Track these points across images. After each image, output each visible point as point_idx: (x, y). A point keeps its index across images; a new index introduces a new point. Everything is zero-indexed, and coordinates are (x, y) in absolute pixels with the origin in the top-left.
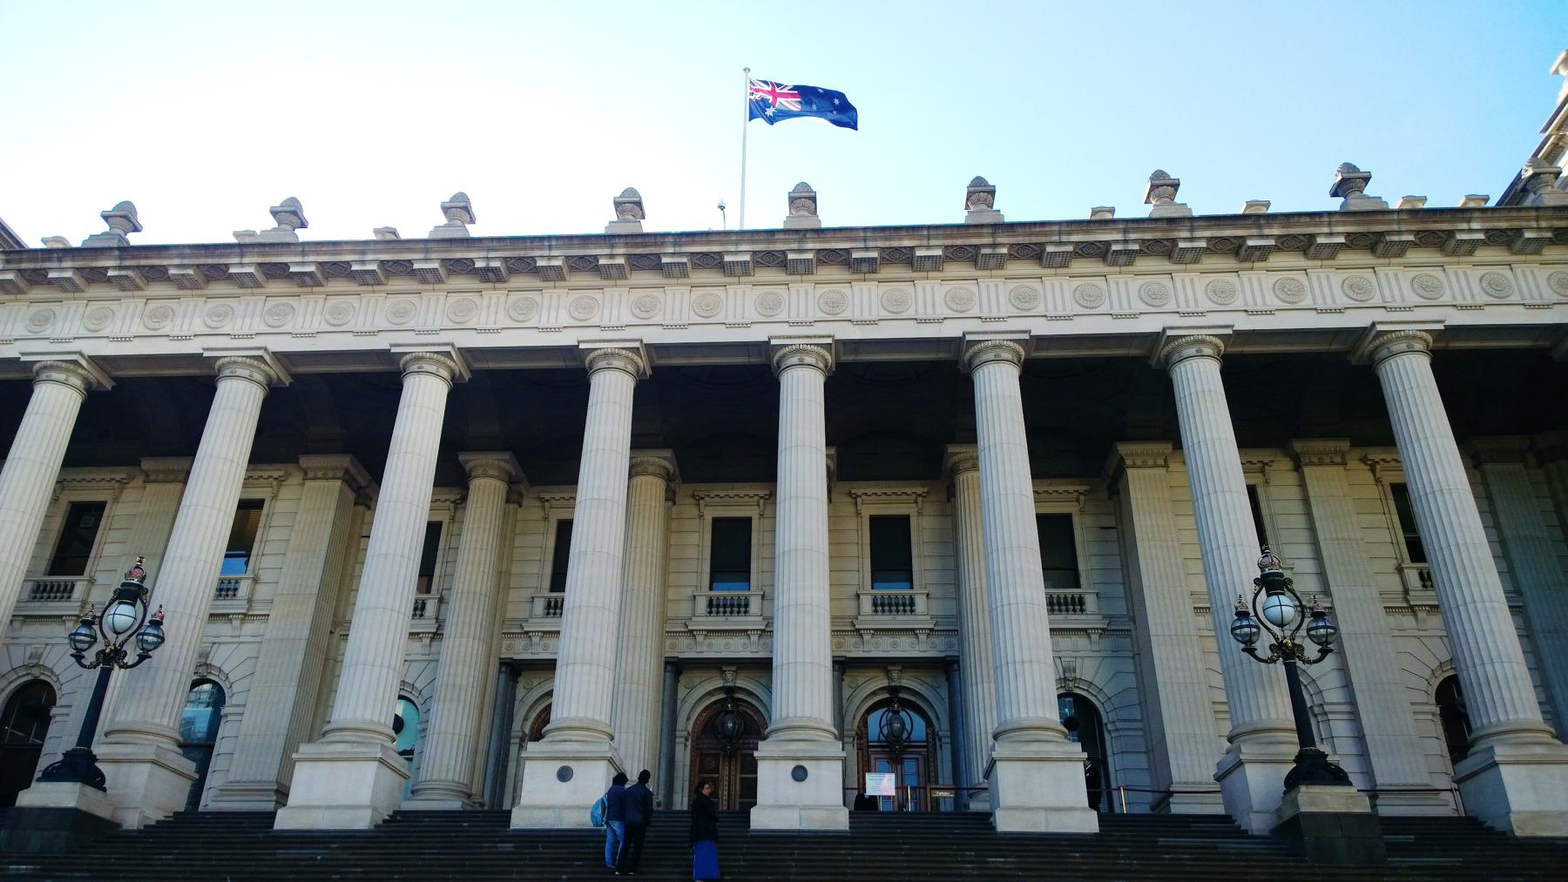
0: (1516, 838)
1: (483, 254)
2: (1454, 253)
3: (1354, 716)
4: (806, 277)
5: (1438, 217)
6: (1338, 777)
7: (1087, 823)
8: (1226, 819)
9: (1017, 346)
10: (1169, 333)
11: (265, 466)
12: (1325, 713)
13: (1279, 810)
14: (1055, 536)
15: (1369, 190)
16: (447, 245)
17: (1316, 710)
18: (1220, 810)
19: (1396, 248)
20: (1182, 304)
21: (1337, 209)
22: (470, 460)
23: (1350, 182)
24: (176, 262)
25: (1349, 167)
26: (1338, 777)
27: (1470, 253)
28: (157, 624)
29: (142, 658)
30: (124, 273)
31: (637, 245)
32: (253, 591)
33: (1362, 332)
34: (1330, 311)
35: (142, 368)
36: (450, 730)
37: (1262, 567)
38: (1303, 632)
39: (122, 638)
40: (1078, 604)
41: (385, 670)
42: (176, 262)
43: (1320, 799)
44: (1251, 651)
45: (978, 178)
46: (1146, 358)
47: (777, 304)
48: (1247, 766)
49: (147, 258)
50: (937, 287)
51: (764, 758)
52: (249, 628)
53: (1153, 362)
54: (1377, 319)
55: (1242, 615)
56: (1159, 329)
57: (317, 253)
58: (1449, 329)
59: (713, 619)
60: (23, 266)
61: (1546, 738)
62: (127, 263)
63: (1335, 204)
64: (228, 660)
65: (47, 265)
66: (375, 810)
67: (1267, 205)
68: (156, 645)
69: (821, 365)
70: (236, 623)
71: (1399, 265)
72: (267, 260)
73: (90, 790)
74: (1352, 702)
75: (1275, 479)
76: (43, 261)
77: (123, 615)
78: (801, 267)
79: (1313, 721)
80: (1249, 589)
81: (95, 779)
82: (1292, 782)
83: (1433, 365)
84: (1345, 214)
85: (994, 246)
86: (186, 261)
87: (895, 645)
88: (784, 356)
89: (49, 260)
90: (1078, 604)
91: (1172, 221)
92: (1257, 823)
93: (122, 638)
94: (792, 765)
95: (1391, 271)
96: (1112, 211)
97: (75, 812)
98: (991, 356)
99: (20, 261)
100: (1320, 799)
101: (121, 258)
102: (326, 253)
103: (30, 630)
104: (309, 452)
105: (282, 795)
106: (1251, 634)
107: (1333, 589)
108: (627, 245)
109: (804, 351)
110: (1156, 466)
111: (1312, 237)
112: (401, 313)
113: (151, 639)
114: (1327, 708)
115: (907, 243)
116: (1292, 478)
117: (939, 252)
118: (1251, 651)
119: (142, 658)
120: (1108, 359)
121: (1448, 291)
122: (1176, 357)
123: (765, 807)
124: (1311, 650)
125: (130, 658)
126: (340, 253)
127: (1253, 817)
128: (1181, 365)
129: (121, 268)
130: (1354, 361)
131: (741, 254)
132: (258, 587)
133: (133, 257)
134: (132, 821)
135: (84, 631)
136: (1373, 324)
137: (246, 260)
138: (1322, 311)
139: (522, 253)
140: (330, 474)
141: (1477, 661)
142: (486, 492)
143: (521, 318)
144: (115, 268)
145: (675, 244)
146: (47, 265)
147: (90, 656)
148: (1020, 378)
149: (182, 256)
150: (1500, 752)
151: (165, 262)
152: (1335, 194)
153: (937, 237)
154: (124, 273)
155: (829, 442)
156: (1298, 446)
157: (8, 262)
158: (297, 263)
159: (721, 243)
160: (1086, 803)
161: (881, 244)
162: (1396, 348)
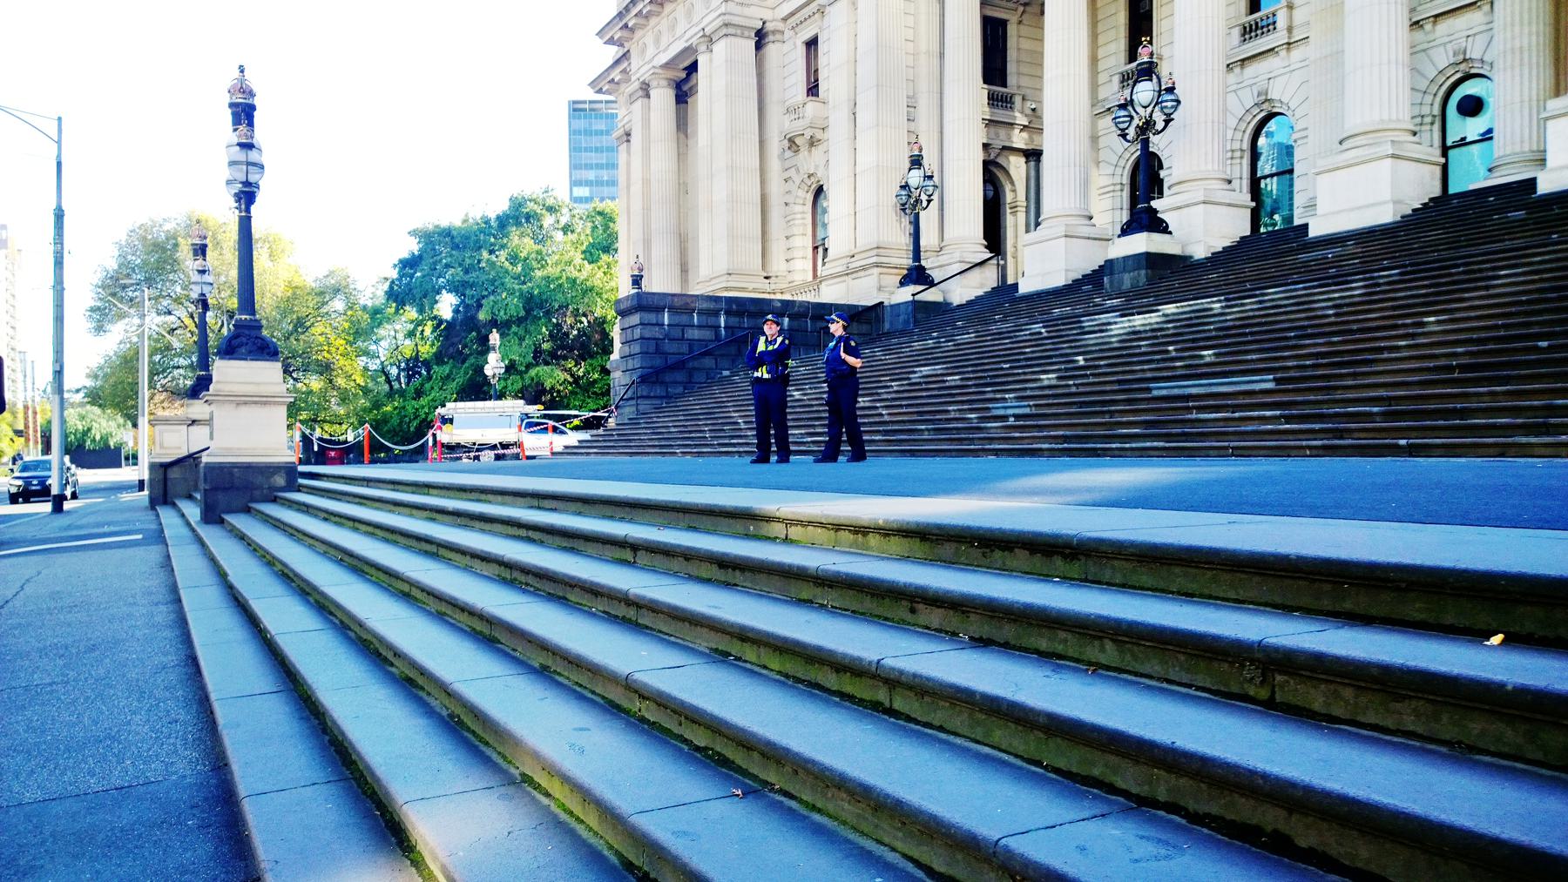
17: (1238, 154)
28: (1171, 90)
29: (1167, 122)
32: (1291, 18)
36: (1517, 99)
41: (1393, 66)
44: (1124, 136)
52: (1297, 53)
66: (1395, 202)
68: (1176, 108)
70: (1283, 53)
73: (1155, 236)
77: (1145, 92)
81: (1159, 226)
97: (1148, 255)
103: (1252, 69)
105: (1542, 162)
113: (1169, 104)
119: (1167, 122)
125: (1160, 126)
132: (1295, 12)
134: (1200, 252)
135: (1123, 113)
147: (1131, 132)
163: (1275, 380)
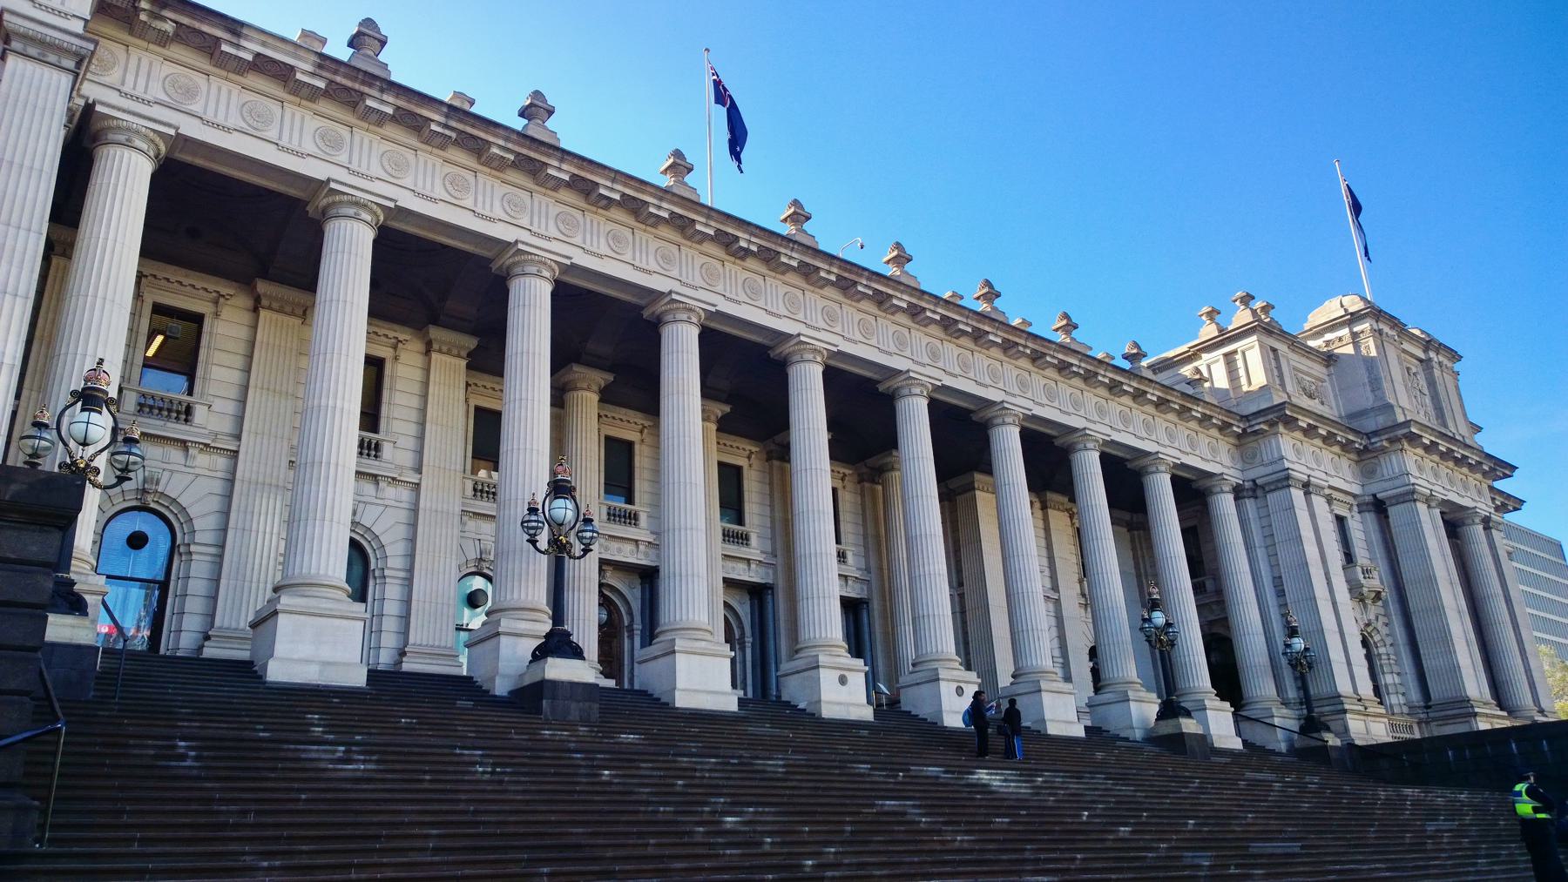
0: (820, 718)
1: (746, 236)
2: (689, 238)
3: (408, 582)
4: (436, 151)
5: (534, 146)
6: (577, 653)
7: (867, 714)
8: (248, 664)
9: (379, 211)
10: (520, 246)
11: (396, 327)
12: (190, 553)
13: (521, 676)
14: (730, 482)
15: (551, 123)
16: (722, 218)
18: (244, 655)
19: (553, 182)
20: (420, 183)
21: (520, 129)
22: (578, 371)
23: (367, 37)
24: (501, 142)
25: (368, 23)
26: (577, 653)
27: (700, 242)
30: (447, 132)
31: (846, 270)
33: (506, 245)
34: (482, 217)
35: (419, 227)
37: (87, 380)
38: (573, 533)
39: (91, 450)
40: (743, 539)
42: (501, 142)
43: (559, 669)
44: (533, 542)
45: (369, 20)
46: (490, 261)
47: (191, 93)
48: (503, 639)
49: (473, 126)
50: (307, 118)
51: (285, 612)
53: (494, 267)
54: (104, 99)
55: (533, 511)
56: (323, 178)
57: (625, 185)
58: (840, 352)
59: (612, 526)
60: (339, 79)
61: (343, 596)
62: (453, 124)
63: (518, 124)
64: (388, 528)
65: (366, 89)
67: (472, 102)
69: (152, 154)
71: (310, 109)
72: (583, 174)
74: (410, 570)
75: (226, 312)
76: (363, 83)
78: (374, 117)
79: (371, 583)
80: (64, 398)
82: (540, 654)
83: (375, 242)
84: (523, 136)
85: (1025, 347)
86: (510, 146)
87: (619, 550)
88: (340, 202)
89: (370, 86)
90: (743, 539)
91: (370, 79)
92: (501, 688)
93: (91, 450)
94: (955, 685)
95: (368, 137)
96: (472, 102)
98: (533, 269)
99: (335, 72)
100: (559, 669)
101: (447, 116)
102: (631, 187)
104: (265, 275)
106: (536, 528)
107: (424, 469)
108: (840, 267)
109: (364, 206)
110: (459, 356)
111: (855, 283)
112: (336, 144)
114: (193, 548)
115: (219, 33)
116: (418, 360)
117: (390, 110)
118: (533, 542)
120: (589, 292)
121: (202, 102)
122: (333, 212)
123: (282, 659)
124: (577, 549)
126: (643, 192)
127: (498, 681)
128: (522, 279)
129: (446, 126)
130: (1129, 466)
133: (461, 121)
136: (329, 180)
137: (564, 167)
138: (207, 123)
139: (773, 247)
140: (455, 352)
141: (328, 516)
142: (587, 402)
143: (457, 194)
144: (439, 124)
145: (868, 279)
146: (366, 89)
148: (153, 176)
149: (507, 139)
150: (680, 644)
151: (491, 139)
152: (522, 114)
153: (571, 164)
154: (447, 132)
155: (829, 429)
156: (262, 287)
157: (320, 66)
158: (607, 187)
159: (894, 289)
160: (865, 700)
161: (460, 126)
162: (1008, 420)
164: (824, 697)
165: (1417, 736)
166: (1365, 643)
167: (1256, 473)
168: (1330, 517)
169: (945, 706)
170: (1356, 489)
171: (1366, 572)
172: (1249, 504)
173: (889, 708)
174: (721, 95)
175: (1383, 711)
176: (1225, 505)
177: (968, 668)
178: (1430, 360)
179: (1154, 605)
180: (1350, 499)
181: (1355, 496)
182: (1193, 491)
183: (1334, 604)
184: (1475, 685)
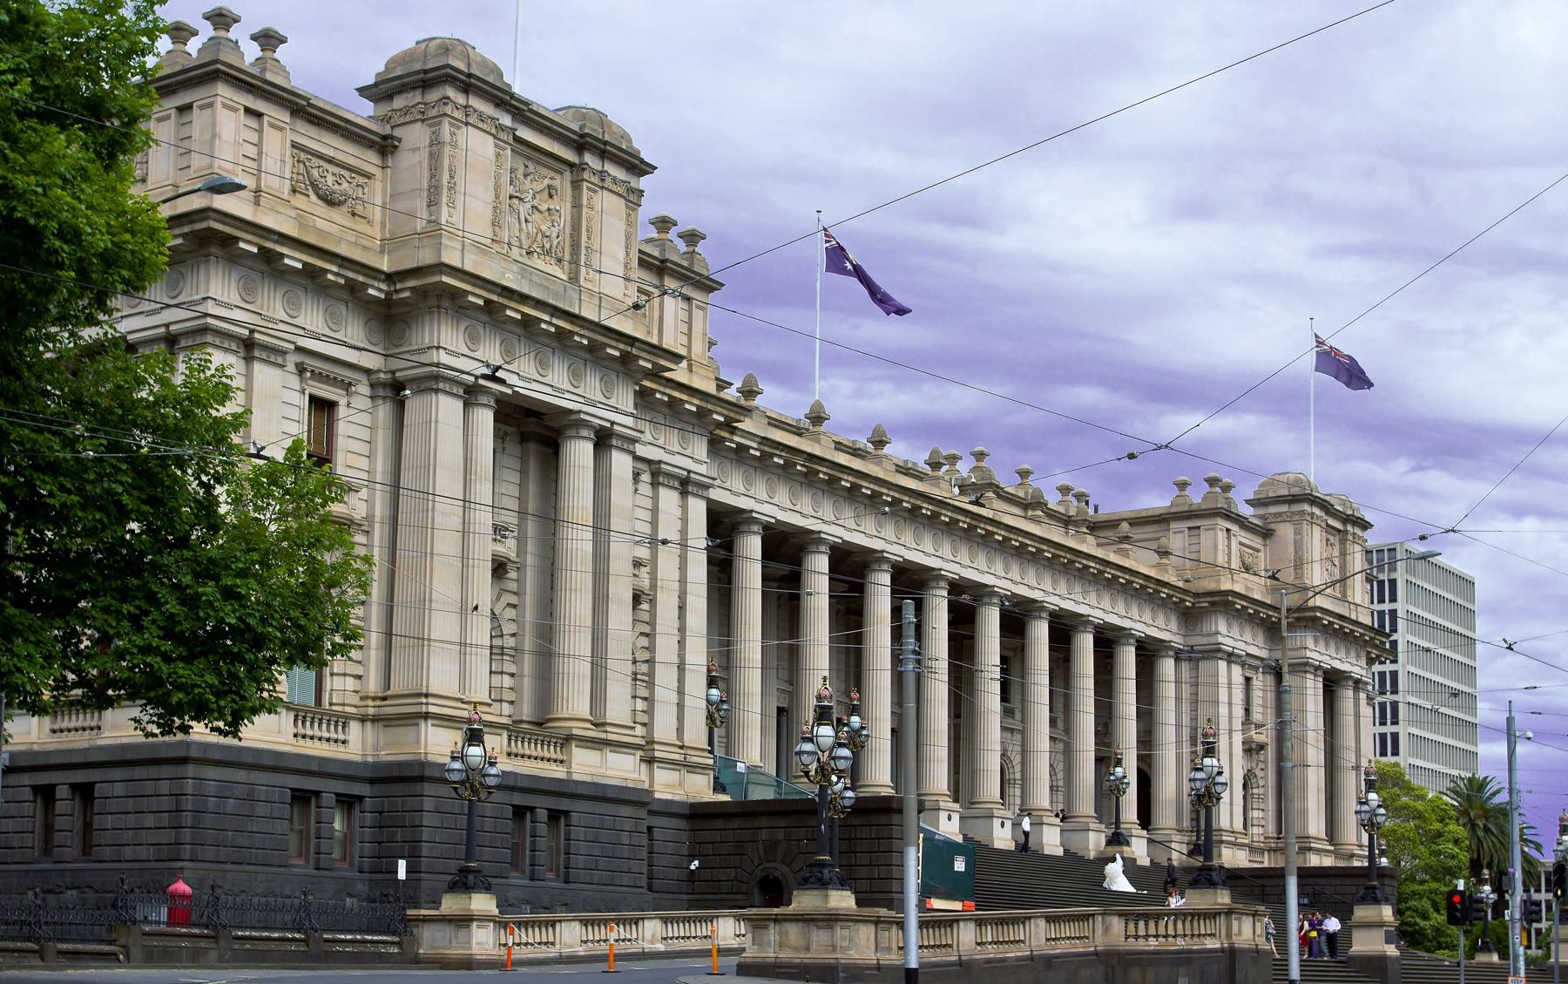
42: (335, 269)
131: (294, 260)
161: (485, 294)
163: (589, 339)
164: (1045, 841)
165: (1266, 865)
166: (1245, 786)
167: (1196, 640)
168: (1241, 680)
169: (995, 834)
170: (1264, 654)
171: (1258, 726)
172: (1185, 666)
173: (1023, 847)
174: (901, 311)
175: (711, 762)
176: (1167, 667)
177: (956, 800)
178: (1346, 532)
179: (855, 710)
180: (1258, 663)
181: (1262, 659)
182: (1148, 652)
183: (1231, 755)
184: (1316, 826)
